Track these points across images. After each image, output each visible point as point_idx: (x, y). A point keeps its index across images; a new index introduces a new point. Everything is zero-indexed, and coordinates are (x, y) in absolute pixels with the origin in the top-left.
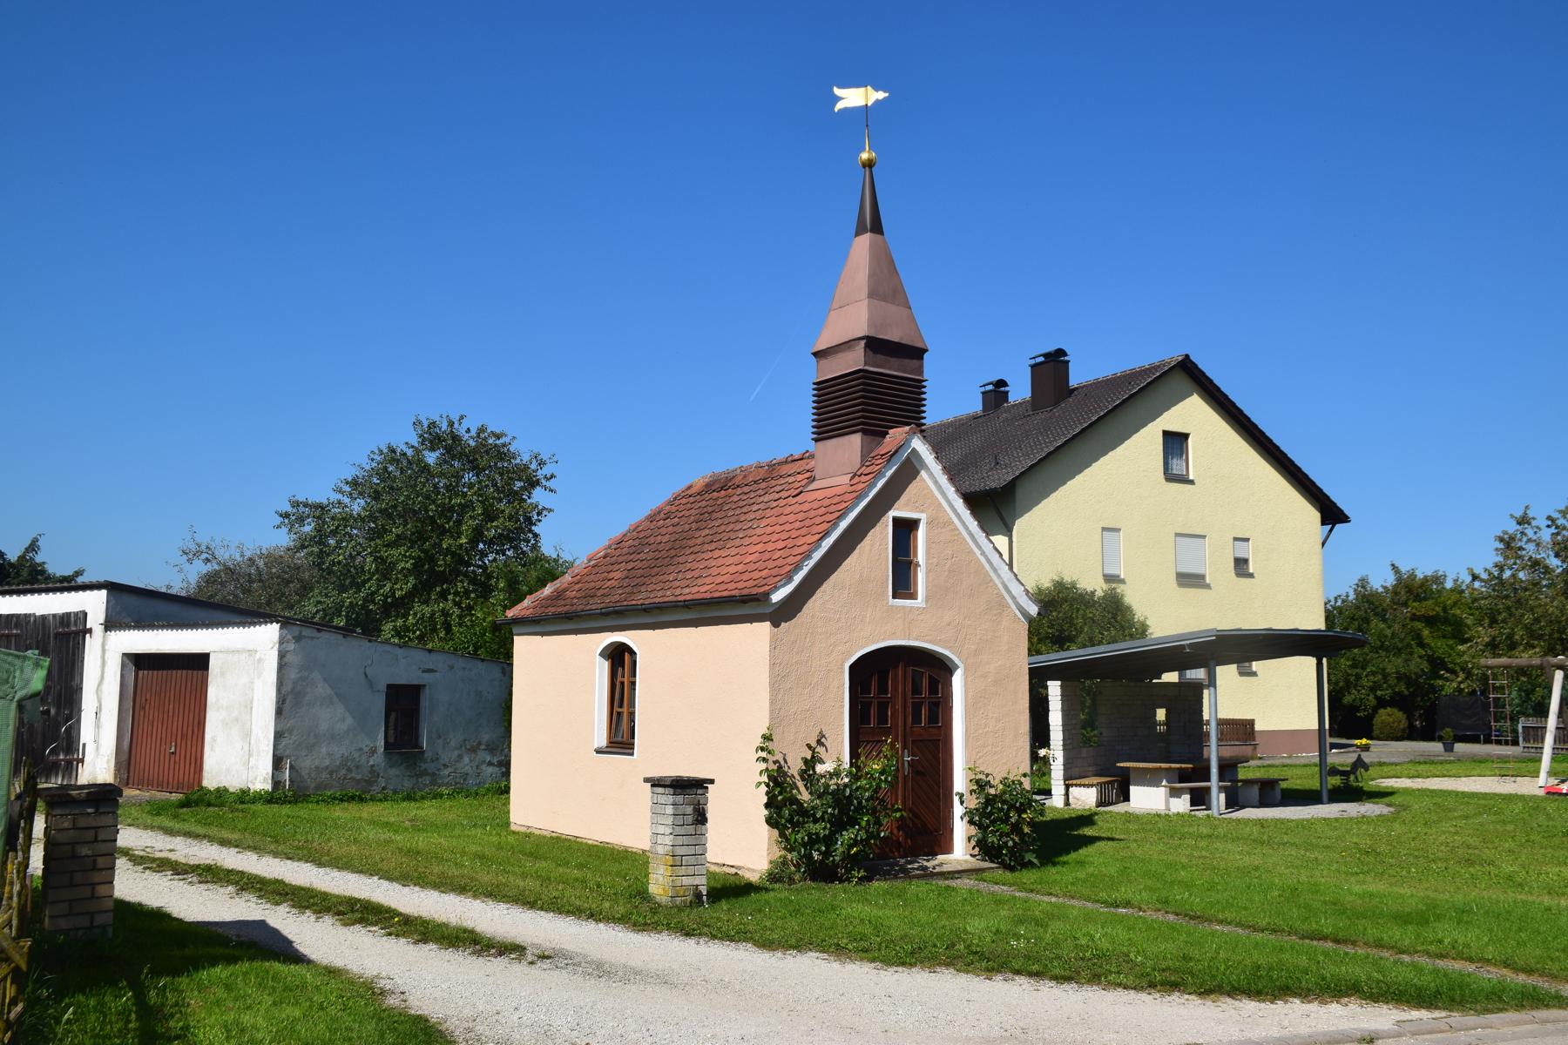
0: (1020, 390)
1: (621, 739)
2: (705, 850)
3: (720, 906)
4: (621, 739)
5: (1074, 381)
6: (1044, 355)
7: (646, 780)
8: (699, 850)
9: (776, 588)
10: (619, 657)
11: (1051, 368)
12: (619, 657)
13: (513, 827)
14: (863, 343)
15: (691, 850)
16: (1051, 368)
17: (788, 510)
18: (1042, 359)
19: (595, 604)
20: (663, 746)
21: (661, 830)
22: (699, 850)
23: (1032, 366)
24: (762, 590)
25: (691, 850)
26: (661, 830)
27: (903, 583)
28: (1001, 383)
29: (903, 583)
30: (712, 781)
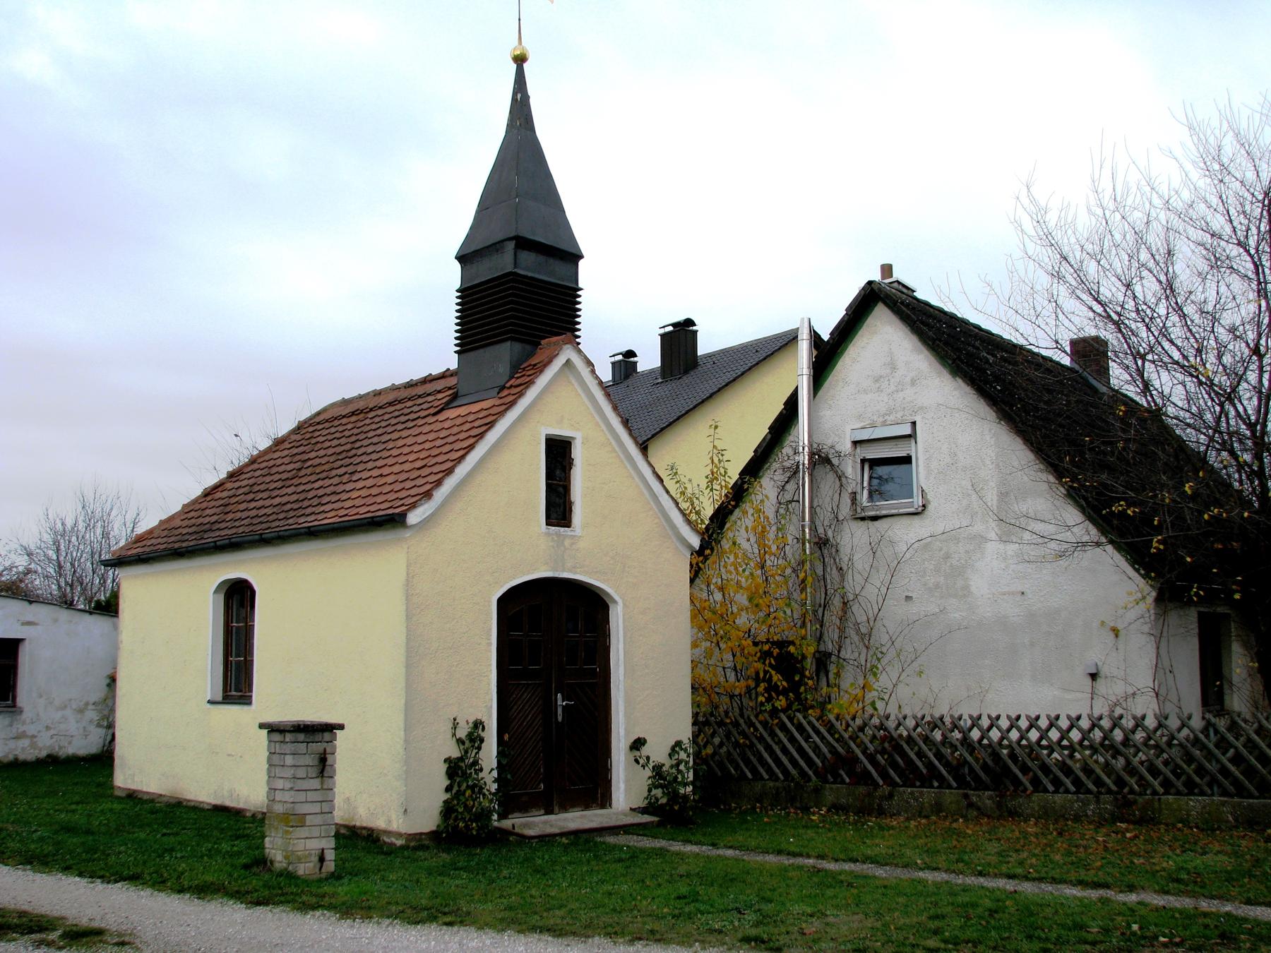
0: (649, 359)
1: (236, 682)
2: (333, 808)
3: (364, 869)
4: (236, 682)
5: (701, 351)
6: (674, 325)
7: (262, 726)
8: (326, 808)
9: (414, 506)
10: (239, 598)
11: (680, 339)
12: (239, 598)
13: (117, 793)
14: (511, 245)
15: (316, 808)
16: (680, 339)
17: (426, 429)
18: (671, 328)
19: (210, 538)
20: (279, 691)
21: (280, 784)
22: (326, 808)
23: (662, 336)
24: (397, 511)
25: (316, 808)
26: (280, 784)
27: (559, 509)
28: (630, 354)
29: (559, 509)
30: (341, 727)
